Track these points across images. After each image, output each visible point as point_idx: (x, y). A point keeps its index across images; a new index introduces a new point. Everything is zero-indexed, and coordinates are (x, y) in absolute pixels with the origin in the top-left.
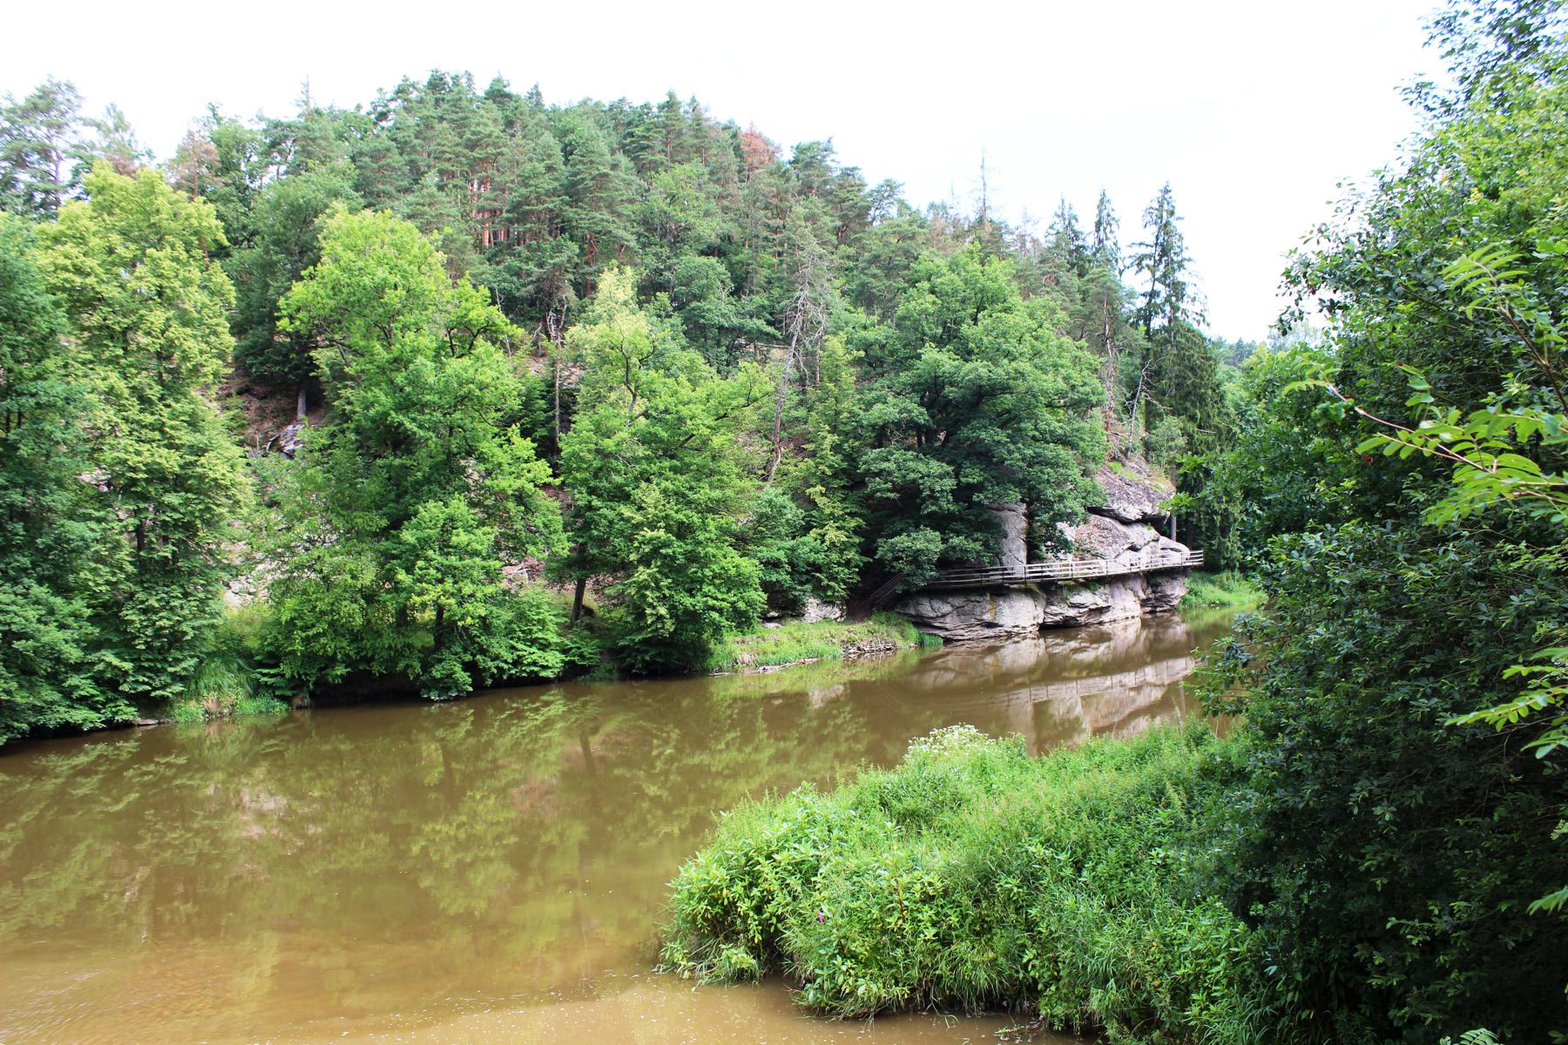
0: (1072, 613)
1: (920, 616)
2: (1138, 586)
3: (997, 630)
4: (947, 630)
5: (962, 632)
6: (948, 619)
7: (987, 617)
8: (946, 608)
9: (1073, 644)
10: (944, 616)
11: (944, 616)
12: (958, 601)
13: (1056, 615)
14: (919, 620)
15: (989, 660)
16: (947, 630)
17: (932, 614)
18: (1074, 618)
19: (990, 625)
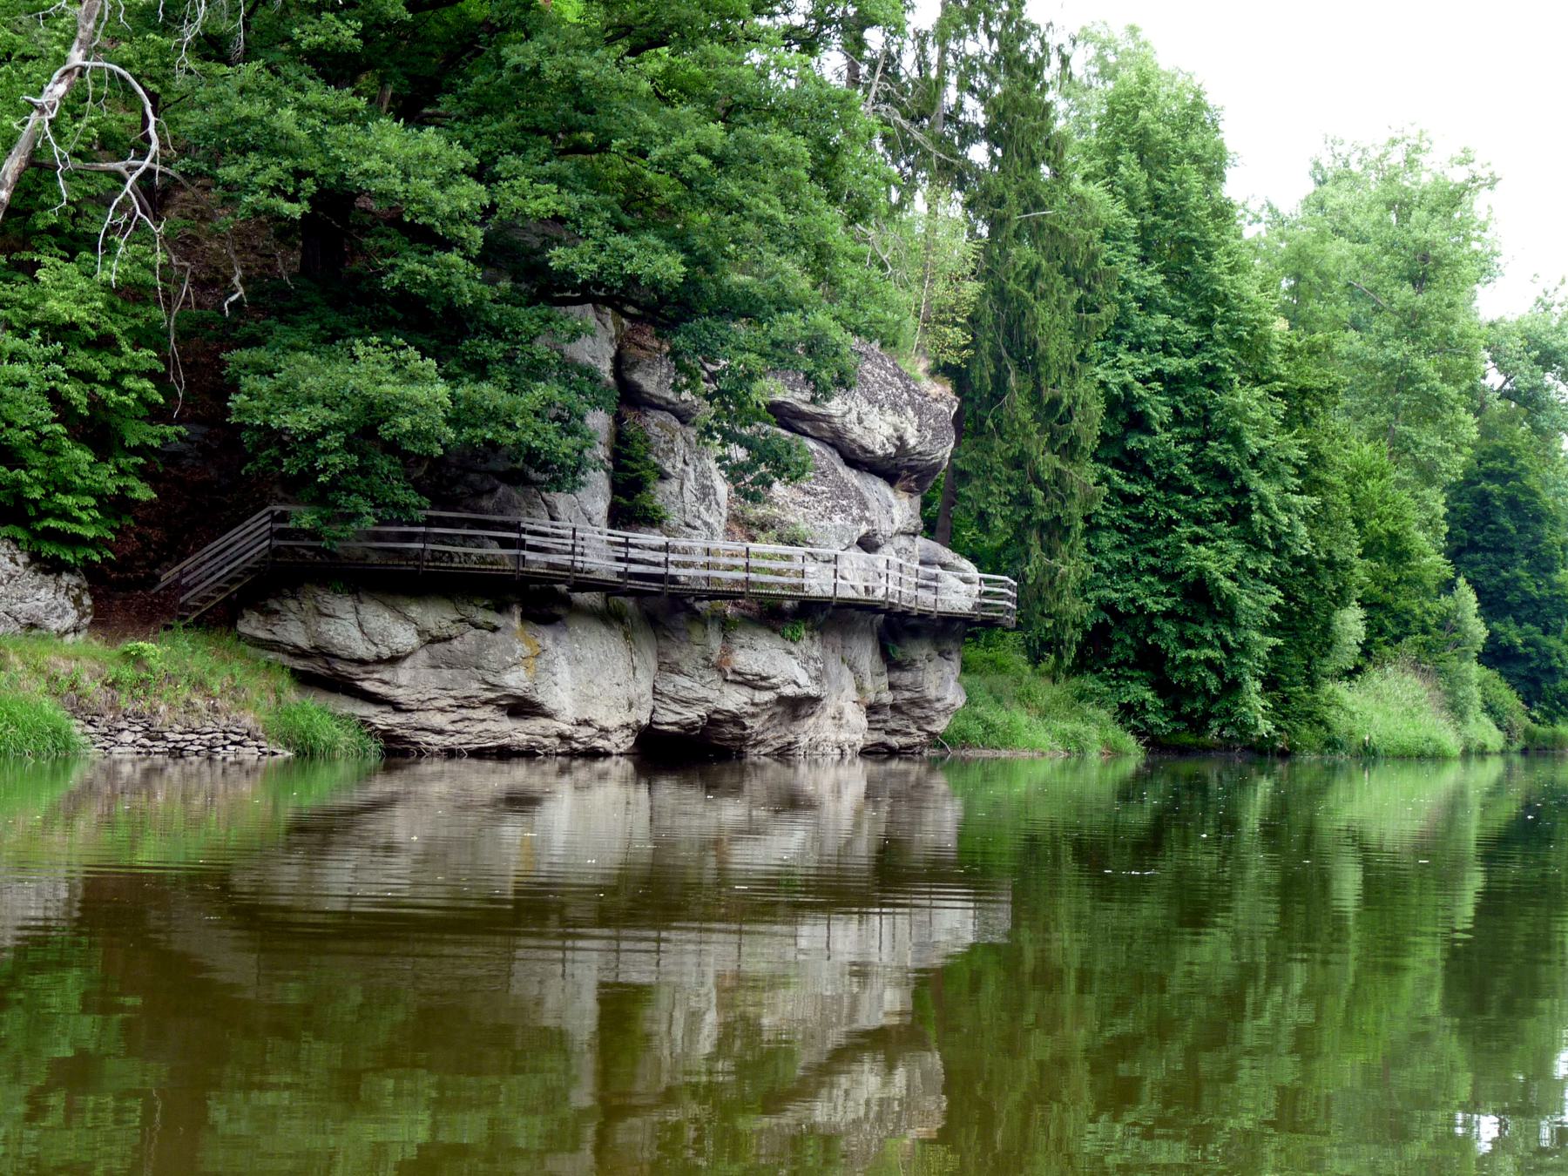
0: (734, 700)
1: (322, 652)
2: (866, 655)
3: (536, 725)
4: (397, 707)
5: (438, 720)
6: (404, 674)
7: (515, 681)
8: (403, 637)
9: (731, 812)
10: (395, 660)
11: (395, 660)
12: (437, 617)
13: (686, 703)
14: (317, 667)
15: (512, 830)
16: (397, 707)
17: (362, 649)
18: (736, 719)
19: (521, 708)
